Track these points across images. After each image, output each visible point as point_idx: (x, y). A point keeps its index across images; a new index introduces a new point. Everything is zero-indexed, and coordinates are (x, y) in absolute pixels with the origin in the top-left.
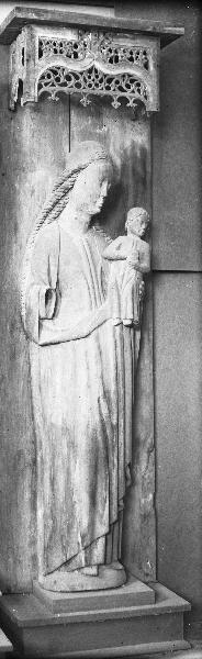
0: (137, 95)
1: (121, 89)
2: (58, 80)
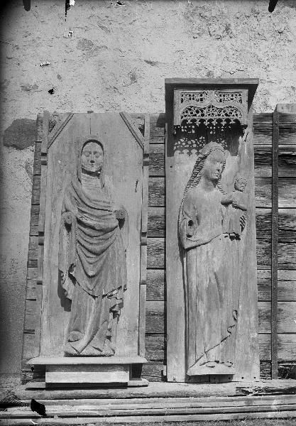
0: (235, 117)
1: (226, 115)
2: (192, 113)
